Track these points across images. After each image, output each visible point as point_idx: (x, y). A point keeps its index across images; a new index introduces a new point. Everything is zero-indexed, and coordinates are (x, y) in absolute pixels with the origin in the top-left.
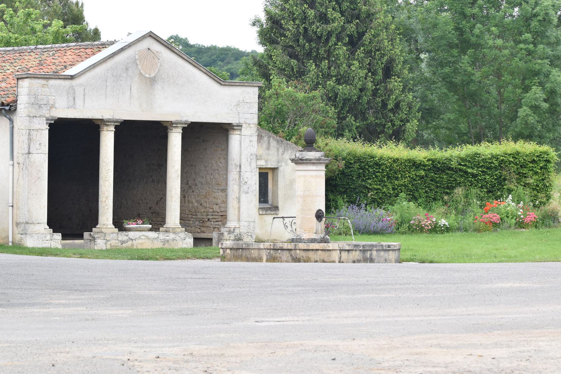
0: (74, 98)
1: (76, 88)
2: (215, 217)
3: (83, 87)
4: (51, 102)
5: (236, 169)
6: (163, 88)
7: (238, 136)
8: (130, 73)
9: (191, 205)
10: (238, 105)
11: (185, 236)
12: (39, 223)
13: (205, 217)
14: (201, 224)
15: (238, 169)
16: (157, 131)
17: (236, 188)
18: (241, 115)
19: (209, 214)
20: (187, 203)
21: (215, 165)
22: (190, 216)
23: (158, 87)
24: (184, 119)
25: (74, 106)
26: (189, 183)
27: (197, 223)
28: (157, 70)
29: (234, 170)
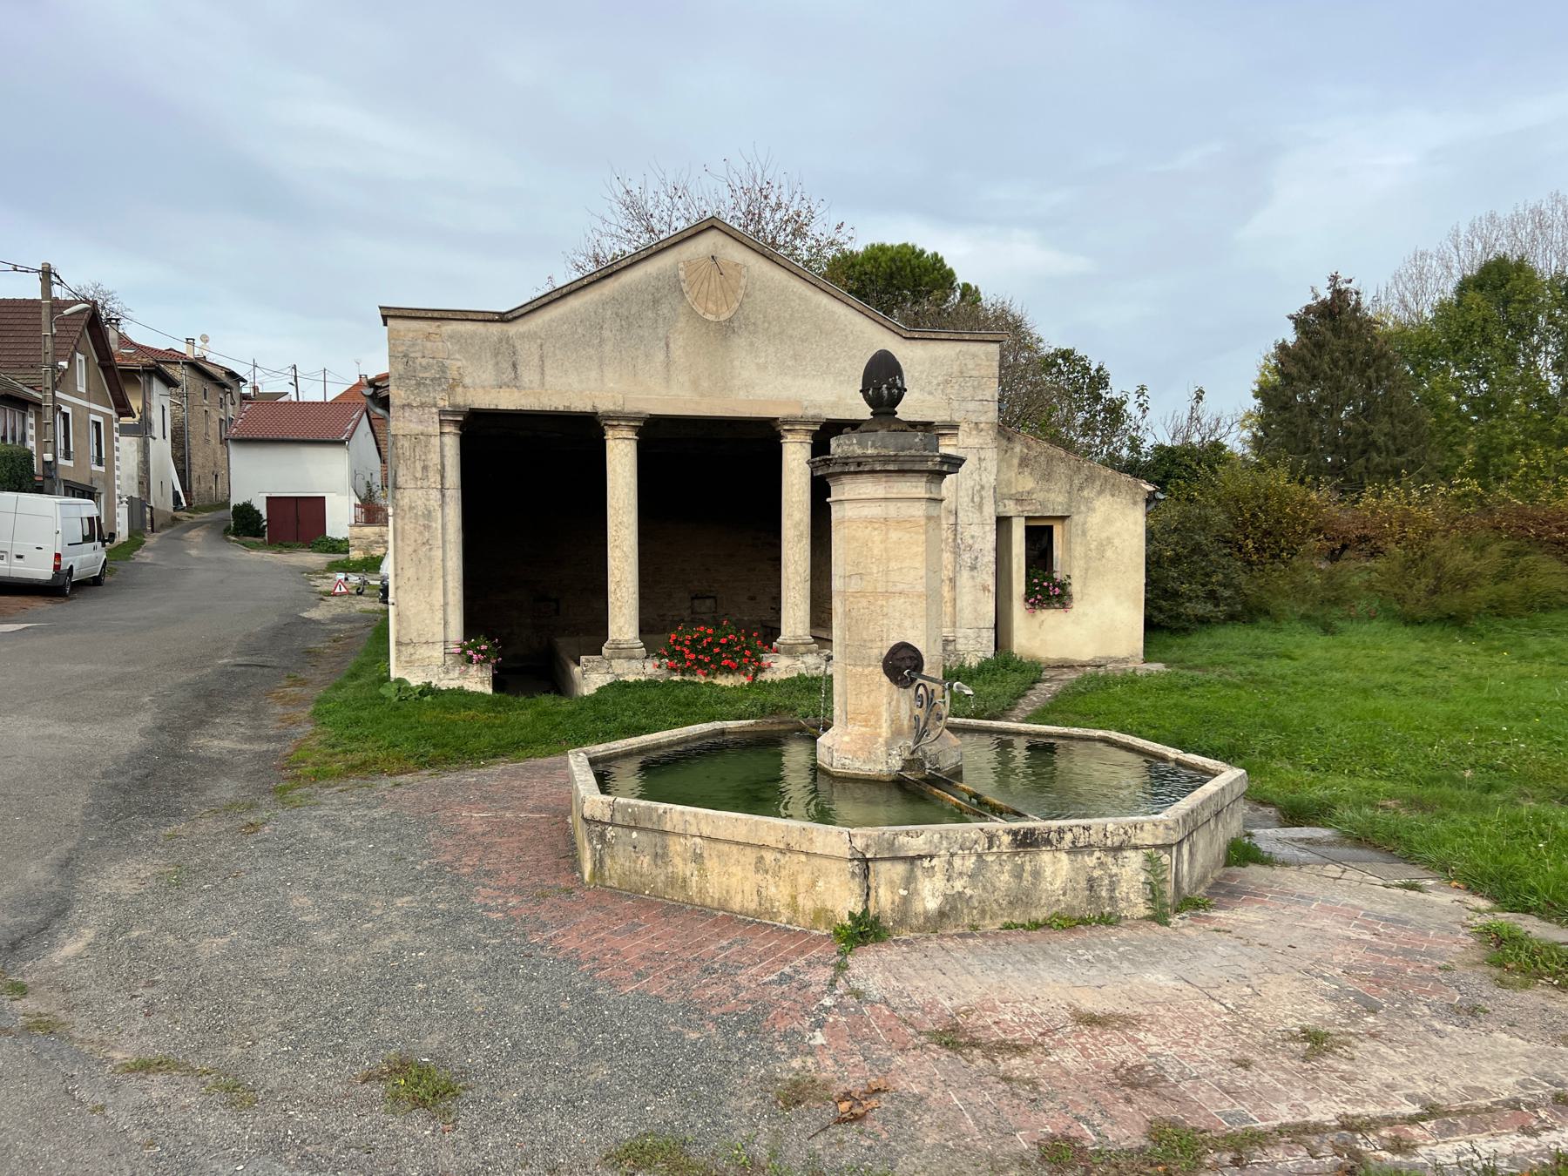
0: (514, 366)
6: (752, 344)
8: (665, 310)
10: (947, 382)
18: (955, 404)
23: (740, 342)
24: (811, 412)
25: (515, 383)
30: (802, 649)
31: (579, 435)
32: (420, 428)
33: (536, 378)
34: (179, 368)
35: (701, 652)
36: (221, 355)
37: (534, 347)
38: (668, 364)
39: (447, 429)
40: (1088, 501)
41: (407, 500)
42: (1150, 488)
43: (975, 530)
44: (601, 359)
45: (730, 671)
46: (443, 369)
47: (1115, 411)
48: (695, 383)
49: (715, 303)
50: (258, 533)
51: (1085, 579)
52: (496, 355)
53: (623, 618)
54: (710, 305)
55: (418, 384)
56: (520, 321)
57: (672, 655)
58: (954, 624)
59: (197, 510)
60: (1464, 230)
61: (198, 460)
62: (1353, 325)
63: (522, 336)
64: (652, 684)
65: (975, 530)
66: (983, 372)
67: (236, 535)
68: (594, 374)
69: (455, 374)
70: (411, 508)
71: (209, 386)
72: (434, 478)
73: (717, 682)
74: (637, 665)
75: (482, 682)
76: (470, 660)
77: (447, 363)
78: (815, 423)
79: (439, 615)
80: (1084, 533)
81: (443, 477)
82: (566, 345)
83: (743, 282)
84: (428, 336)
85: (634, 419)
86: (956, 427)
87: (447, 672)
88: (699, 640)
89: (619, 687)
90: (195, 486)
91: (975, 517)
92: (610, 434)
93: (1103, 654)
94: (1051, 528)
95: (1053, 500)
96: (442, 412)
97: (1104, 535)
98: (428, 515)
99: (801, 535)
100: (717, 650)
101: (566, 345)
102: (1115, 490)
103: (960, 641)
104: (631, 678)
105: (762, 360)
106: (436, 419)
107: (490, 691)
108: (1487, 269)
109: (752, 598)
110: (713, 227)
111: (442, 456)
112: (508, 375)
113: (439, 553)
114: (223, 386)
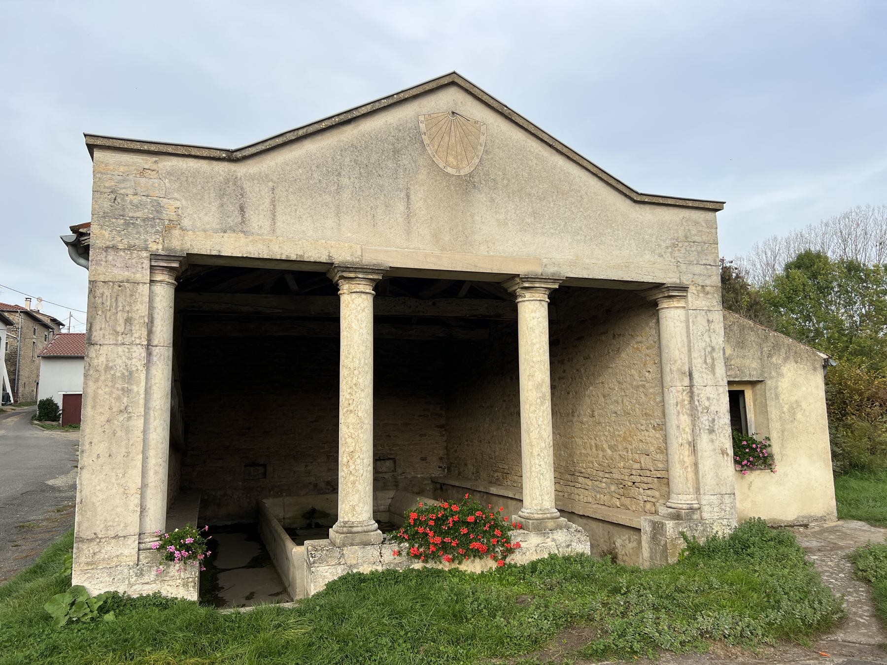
0: (242, 209)
1: (247, 185)
2: (645, 479)
3: (270, 184)
4: (169, 213)
5: (681, 380)
6: (492, 200)
7: (681, 312)
8: (405, 161)
9: (601, 454)
10: (674, 246)
11: (568, 538)
12: (116, 537)
13: (626, 478)
14: (621, 491)
15: (686, 382)
16: (486, 301)
17: (685, 420)
18: (683, 267)
19: (634, 472)
20: (594, 449)
21: (637, 377)
22: (601, 474)
23: (481, 198)
24: (551, 270)
25: (242, 227)
26: (596, 414)
27: (613, 488)
28: (476, 161)
29: (678, 384)
30: (551, 524)
31: (314, 286)
32: (127, 274)
33: (267, 224)
34: (17, 315)
35: (447, 533)
36: (47, 310)
37: (265, 191)
38: (409, 215)
39: (159, 277)
40: (777, 367)
41: (102, 359)
42: (825, 357)
43: (709, 391)
44: (338, 207)
45: (477, 554)
46: (158, 208)
47: (852, 268)
48: (436, 237)
49: (456, 157)
50: (56, 419)
51: (783, 439)
52: (221, 197)
53: (355, 496)
54: (451, 159)
55: (127, 224)
56: (250, 162)
57: (412, 538)
58: (698, 490)
59: (21, 405)
60: (761, 245)
61: (24, 374)
62: (737, 286)
63: (252, 178)
64: (389, 577)
65: (709, 391)
66: (704, 238)
67: (40, 420)
68: (330, 223)
69: (173, 216)
70: (108, 368)
71: (38, 327)
72: (139, 333)
73: (463, 567)
74: (372, 552)
75: (185, 585)
76: (171, 557)
77: (164, 202)
78: (555, 281)
79: (135, 500)
80: (777, 397)
81: (150, 332)
82: (300, 190)
83: (482, 139)
84: (143, 172)
85: (374, 271)
86: (685, 289)
87: (141, 574)
88: (444, 519)
89: (353, 583)
90: (21, 389)
91: (709, 378)
92: (345, 288)
93: (805, 513)
94: (743, 392)
95: (751, 368)
96: (154, 256)
97: (793, 399)
98: (129, 376)
99: (544, 397)
100: (464, 530)
101: (300, 190)
102: (798, 357)
103: (706, 508)
104: (366, 569)
105: (502, 217)
106: (147, 264)
107: (193, 595)
108: (800, 257)
109: (423, 459)
110: (453, 83)
111: (151, 308)
112: (236, 218)
113: (140, 423)
114: (46, 326)
